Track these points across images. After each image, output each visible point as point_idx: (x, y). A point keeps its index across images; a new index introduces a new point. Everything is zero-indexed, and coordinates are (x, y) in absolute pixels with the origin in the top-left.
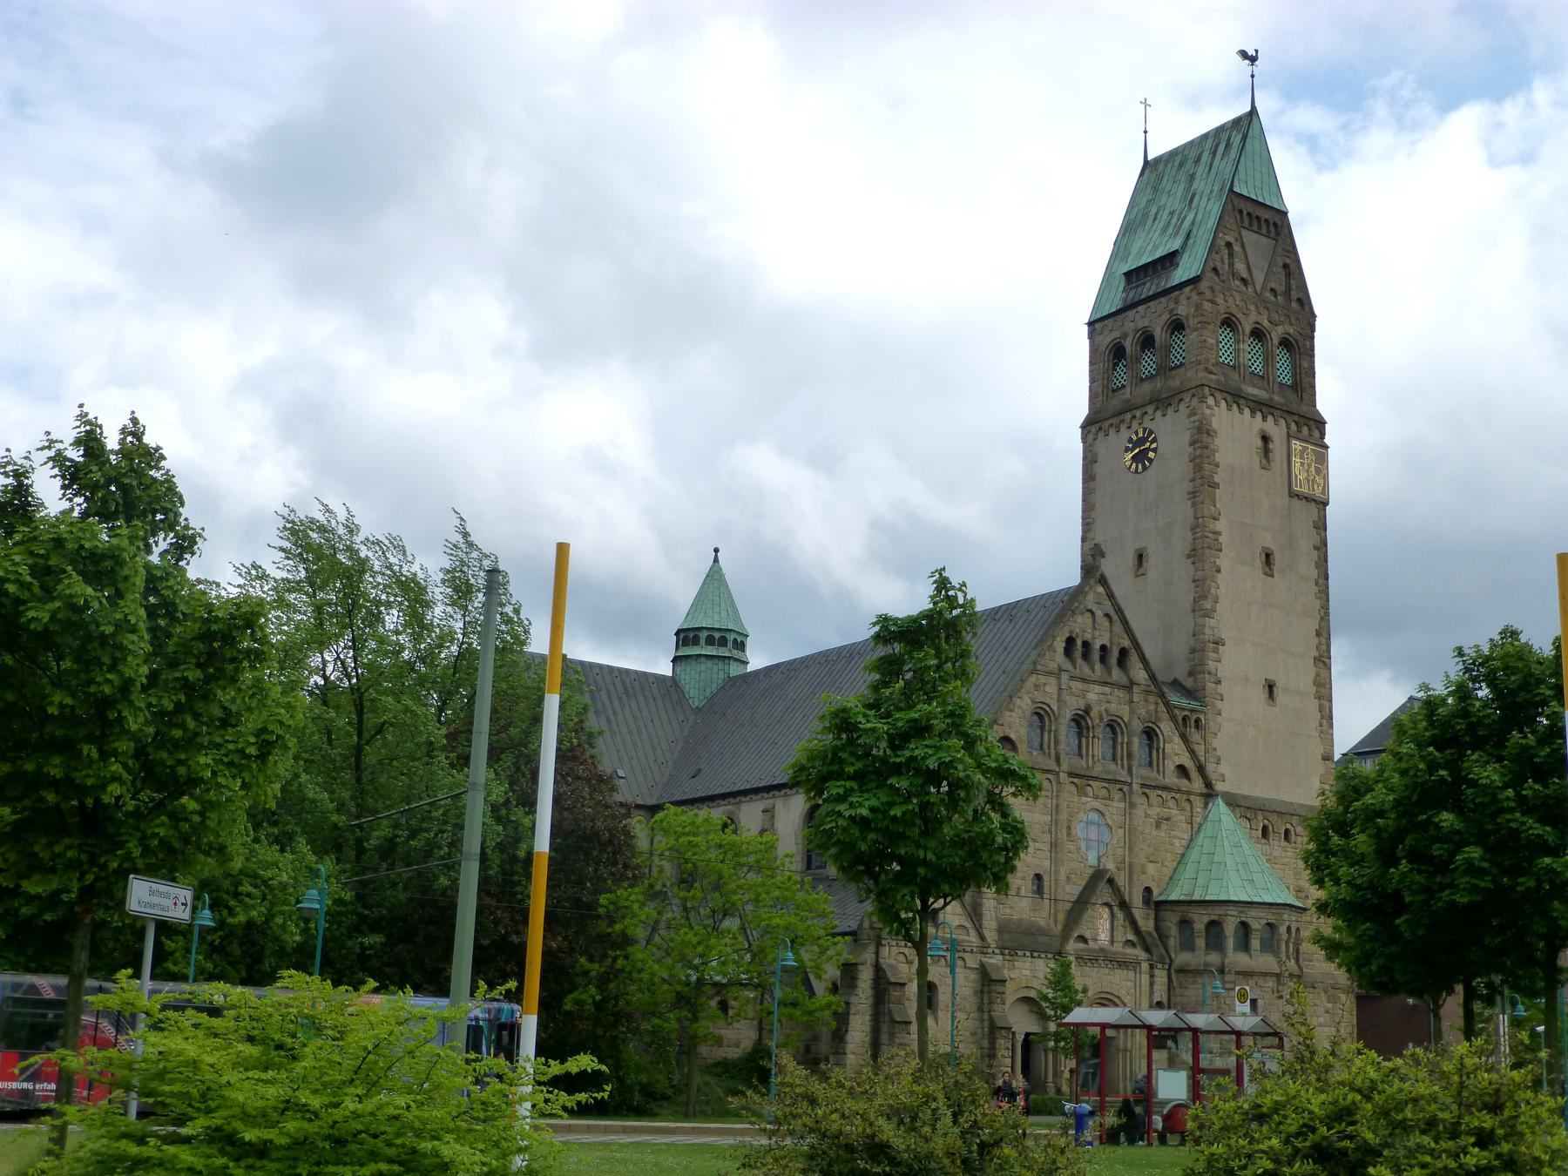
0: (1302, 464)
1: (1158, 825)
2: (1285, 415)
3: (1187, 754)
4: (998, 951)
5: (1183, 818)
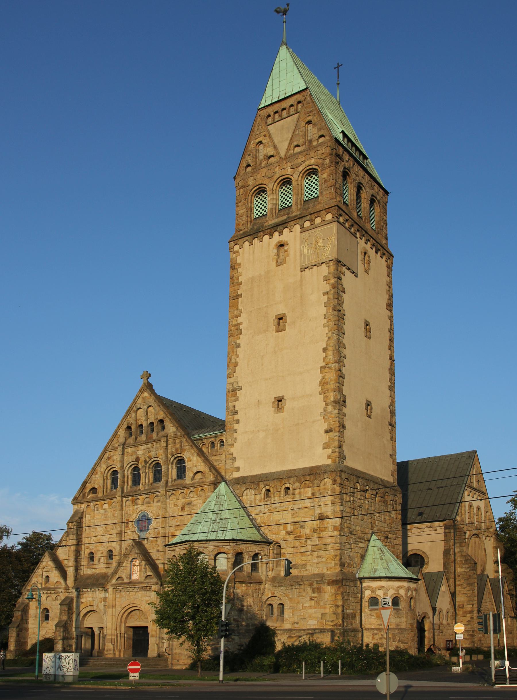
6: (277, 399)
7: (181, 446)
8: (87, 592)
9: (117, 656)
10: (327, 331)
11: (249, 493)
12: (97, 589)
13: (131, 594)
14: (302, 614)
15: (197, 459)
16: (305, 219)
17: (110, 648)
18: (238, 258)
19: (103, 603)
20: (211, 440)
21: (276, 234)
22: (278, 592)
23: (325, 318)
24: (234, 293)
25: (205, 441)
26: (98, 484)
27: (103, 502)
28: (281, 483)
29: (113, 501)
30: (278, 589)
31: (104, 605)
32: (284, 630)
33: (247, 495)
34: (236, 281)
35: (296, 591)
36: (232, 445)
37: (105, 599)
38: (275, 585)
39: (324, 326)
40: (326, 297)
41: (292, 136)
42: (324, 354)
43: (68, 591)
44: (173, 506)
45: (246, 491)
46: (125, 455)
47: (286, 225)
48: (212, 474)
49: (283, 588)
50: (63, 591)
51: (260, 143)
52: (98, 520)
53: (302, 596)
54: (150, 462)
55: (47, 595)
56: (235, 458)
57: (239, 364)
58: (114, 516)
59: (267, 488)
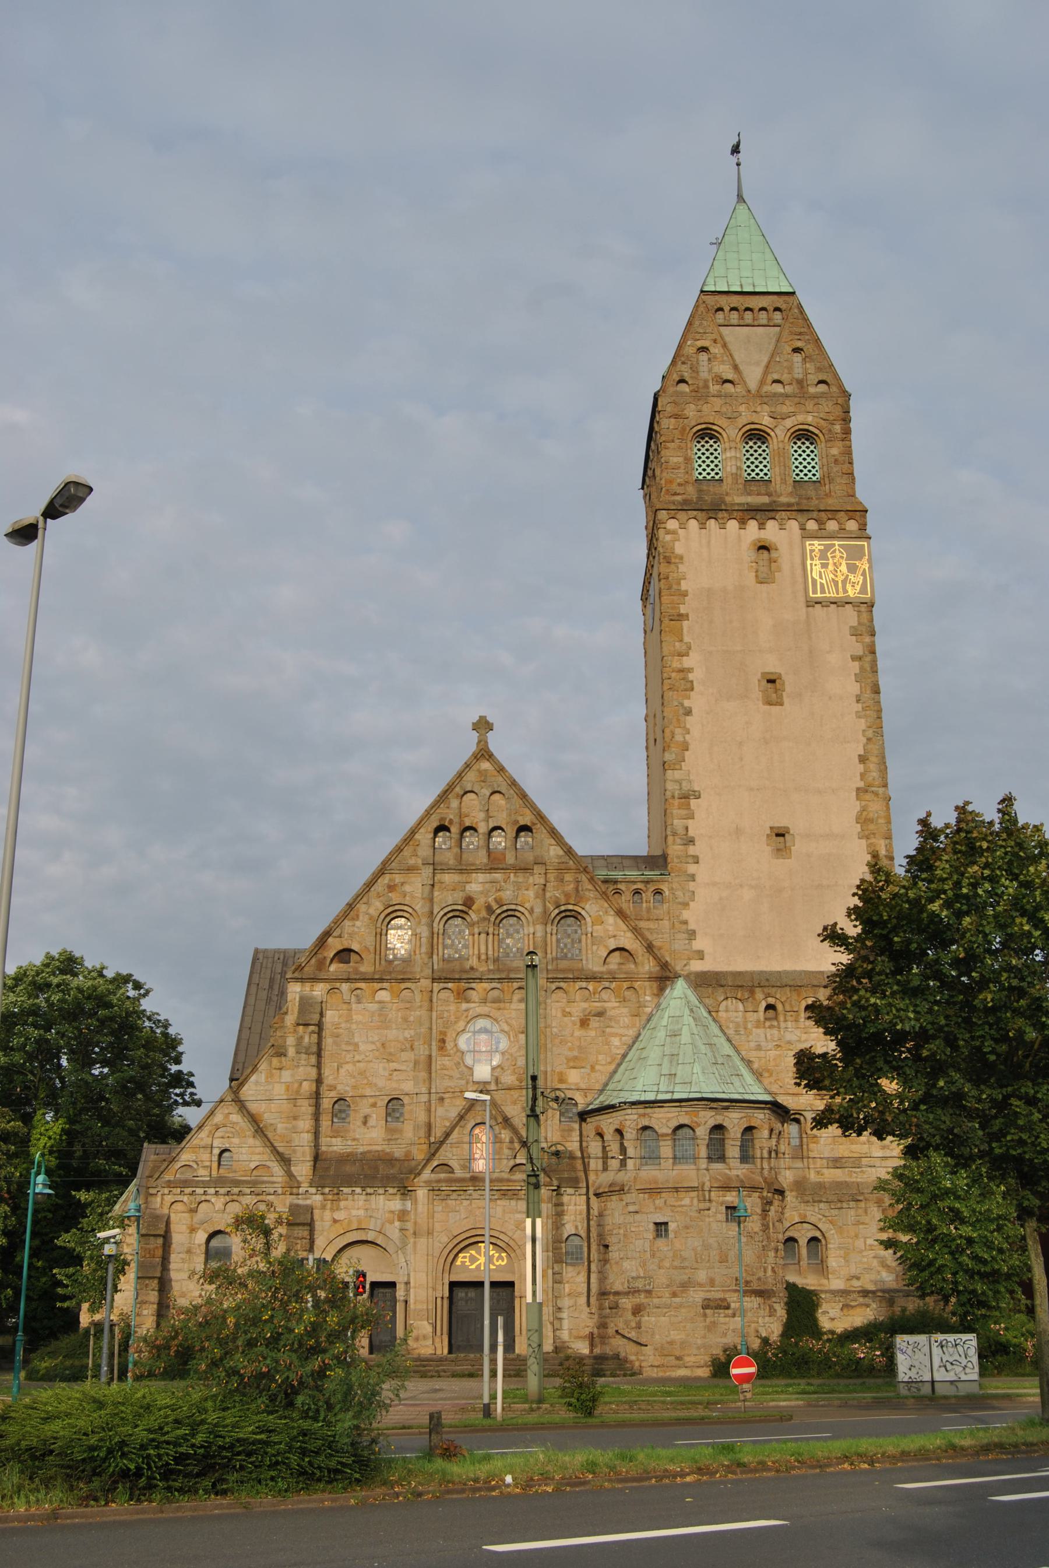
0: (825, 566)
1: (584, 1023)
2: (753, 514)
3: (629, 934)
4: (313, 1190)
5: (625, 1011)
6: (776, 831)
7: (577, 889)
8: (350, 1197)
9: (439, 1352)
10: (864, 727)
11: (732, 1008)
12: (381, 1191)
13: (474, 1206)
14: (865, 1260)
15: (616, 923)
16: (810, 515)
17: (425, 1332)
18: (677, 544)
19: (397, 1224)
20: (635, 887)
21: (753, 524)
22: (813, 1214)
23: (858, 701)
24: (673, 608)
25: (622, 886)
26: (360, 943)
27: (377, 986)
28: (799, 995)
29: (403, 986)
30: (811, 1208)
31: (401, 1230)
32: (834, 1293)
33: (727, 1011)
34: (675, 587)
35: (852, 1212)
36: (686, 905)
37: (403, 1215)
38: (806, 1198)
39: (858, 715)
40: (856, 664)
41: (769, 362)
42: (862, 766)
43: (295, 1190)
44: (559, 1015)
45: (724, 1003)
46: (436, 887)
47: (772, 514)
48: (651, 958)
49: (822, 1205)
50: (280, 1191)
51: (704, 349)
52: (360, 1026)
53: (863, 1223)
54: (498, 911)
55: (228, 1198)
56: (694, 932)
57: (690, 747)
58: (405, 1020)
59: (771, 1001)
